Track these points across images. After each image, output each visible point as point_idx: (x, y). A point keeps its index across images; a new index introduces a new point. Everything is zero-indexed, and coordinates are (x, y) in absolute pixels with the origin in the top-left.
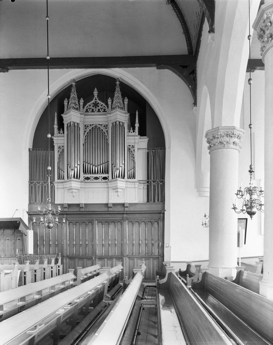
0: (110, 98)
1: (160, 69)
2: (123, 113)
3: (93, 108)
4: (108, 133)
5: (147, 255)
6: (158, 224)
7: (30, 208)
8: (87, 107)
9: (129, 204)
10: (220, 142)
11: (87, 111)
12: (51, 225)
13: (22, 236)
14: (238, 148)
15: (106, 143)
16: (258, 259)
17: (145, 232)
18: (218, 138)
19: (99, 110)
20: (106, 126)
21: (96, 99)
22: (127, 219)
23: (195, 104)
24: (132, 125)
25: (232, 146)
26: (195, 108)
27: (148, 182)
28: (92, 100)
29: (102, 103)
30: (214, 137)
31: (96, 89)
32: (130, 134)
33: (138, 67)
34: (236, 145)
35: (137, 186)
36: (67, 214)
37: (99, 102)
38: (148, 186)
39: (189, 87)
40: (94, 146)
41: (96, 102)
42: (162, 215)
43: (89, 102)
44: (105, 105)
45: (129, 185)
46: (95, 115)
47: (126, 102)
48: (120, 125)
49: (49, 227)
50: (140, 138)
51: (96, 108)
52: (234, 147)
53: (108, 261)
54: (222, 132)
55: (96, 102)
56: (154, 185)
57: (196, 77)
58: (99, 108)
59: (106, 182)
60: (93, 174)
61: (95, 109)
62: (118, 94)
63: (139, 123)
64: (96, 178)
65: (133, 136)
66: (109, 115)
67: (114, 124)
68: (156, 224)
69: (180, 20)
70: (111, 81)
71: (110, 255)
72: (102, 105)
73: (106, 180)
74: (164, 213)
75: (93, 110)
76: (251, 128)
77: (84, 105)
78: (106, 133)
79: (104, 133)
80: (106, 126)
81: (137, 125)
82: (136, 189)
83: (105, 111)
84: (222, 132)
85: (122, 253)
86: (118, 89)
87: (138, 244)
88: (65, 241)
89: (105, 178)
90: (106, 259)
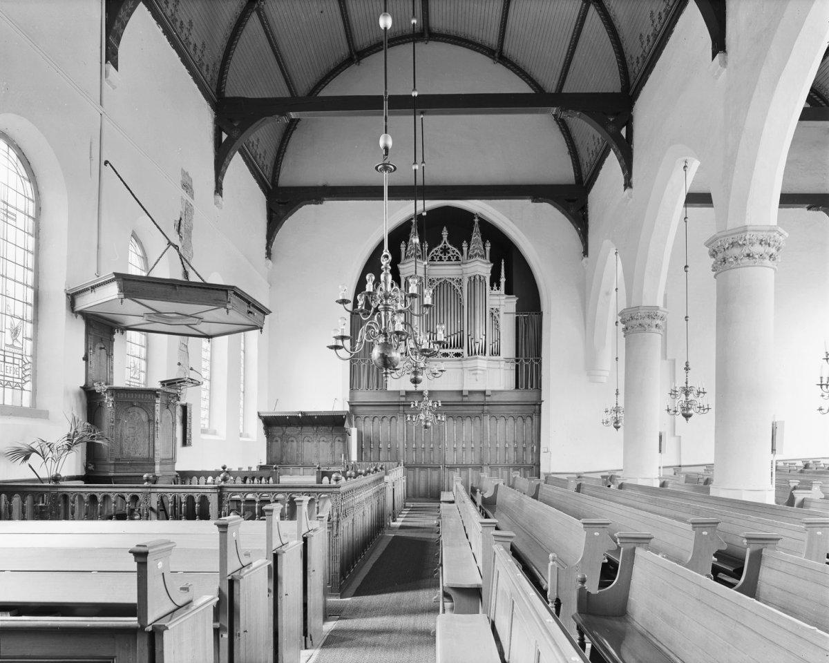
0: (465, 242)
1: (536, 202)
2: (483, 263)
3: (440, 255)
4: (462, 291)
6: (532, 420)
7: (352, 397)
8: (433, 253)
9: (492, 391)
10: (640, 325)
11: (432, 259)
12: (429, 424)
13: (345, 435)
15: (459, 305)
16: (672, 469)
17: (513, 431)
19: (449, 258)
20: (460, 281)
21: (445, 243)
23: (586, 253)
24: (495, 280)
25: (654, 329)
26: (585, 259)
27: (517, 361)
28: (440, 244)
29: (454, 249)
30: (632, 318)
31: (445, 229)
32: (493, 292)
33: (506, 199)
34: (659, 328)
35: (502, 366)
36: (404, 405)
37: (450, 246)
38: (517, 366)
39: (577, 230)
40: (442, 309)
41: (445, 246)
42: (537, 407)
43: (436, 247)
44: (458, 251)
45: (495, 365)
46: (445, 265)
47: (488, 249)
48: (480, 279)
49: (426, 427)
50: (507, 298)
51: (445, 255)
52: (657, 330)
53: (462, 472)
55: (445, 246)
56: (526, 365)
57: (587, 215)
58: (450, 255)
59: (460, 360)
60: (447, 347)
61: (443, 257)
62: (476, 237)
63: (506, 277)
64: (446, 355)
65: (498, 295)
66: (463, 266)
67: (472, 279)
68: (529, 419)
69: (564, 136)
70: (468, 216)
71: (464, 463)
72: (453, 251)
73: (459, 358)
74: (540, 405)
75: (441, 258)
77: (429, 250)
78: (459, 291)
79: (456, 291)
80: (460, 281)
81: (503, 280)
82: (502, 370)
83: (458, 259)
84: (642, 313)
85: (481, 460)
86: (476, 229)
89: (457, 355)
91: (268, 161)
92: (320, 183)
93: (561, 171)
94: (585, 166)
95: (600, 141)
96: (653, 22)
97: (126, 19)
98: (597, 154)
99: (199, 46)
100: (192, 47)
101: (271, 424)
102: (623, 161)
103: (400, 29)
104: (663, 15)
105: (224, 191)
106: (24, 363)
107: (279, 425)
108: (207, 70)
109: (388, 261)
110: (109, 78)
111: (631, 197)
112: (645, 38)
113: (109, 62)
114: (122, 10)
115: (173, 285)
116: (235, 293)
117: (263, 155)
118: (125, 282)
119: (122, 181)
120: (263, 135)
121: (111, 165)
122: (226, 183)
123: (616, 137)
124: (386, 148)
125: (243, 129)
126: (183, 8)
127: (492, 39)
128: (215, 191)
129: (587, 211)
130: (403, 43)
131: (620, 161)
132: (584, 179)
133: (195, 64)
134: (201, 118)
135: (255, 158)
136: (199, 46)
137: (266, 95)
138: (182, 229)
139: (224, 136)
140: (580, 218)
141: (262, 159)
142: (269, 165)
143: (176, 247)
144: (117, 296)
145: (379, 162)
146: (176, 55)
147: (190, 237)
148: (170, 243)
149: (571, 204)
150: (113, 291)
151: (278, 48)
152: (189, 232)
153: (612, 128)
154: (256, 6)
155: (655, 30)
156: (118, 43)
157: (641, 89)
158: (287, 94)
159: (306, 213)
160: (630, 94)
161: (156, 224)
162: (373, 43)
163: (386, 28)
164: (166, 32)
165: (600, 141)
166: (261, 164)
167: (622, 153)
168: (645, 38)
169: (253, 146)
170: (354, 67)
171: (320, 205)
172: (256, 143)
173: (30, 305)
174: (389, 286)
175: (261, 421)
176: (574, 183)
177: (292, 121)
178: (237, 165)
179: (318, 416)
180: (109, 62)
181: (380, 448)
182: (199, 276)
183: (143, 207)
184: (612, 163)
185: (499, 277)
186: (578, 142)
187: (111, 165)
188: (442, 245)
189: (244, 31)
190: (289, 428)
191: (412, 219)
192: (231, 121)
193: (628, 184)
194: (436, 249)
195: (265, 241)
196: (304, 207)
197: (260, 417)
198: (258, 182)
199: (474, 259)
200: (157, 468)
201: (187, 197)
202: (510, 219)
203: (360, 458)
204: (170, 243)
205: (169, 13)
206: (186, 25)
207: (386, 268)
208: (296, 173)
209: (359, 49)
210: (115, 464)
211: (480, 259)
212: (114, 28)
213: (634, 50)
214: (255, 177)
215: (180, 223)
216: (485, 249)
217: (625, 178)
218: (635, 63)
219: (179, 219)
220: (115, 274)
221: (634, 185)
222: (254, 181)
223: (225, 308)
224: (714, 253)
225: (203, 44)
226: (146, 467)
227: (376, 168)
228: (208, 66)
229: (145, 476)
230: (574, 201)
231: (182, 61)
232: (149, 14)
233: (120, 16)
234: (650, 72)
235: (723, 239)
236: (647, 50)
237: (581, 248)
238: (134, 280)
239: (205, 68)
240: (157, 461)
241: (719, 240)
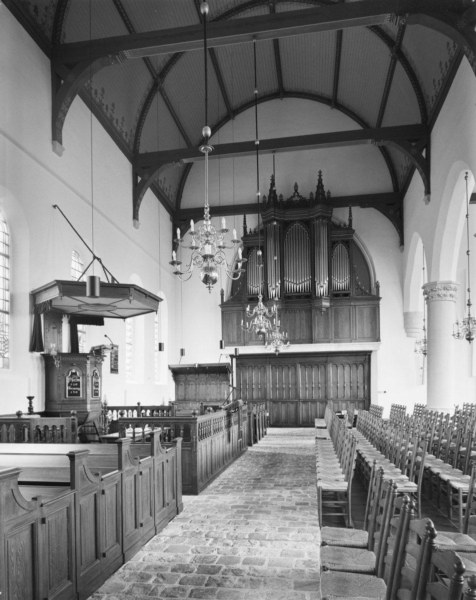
5: (352, 397)
10: (438, 295)
14: (454, 299)
18: (436, 291)
22: (332, 362)
23: (402, 243)
25: (448, 298)
30: (432, 290)
34: (453, 297)
42: (367, 356)
52: (451, 299)
54: (439, 286)
71: (313, 398)
76: (468, 255)
85: (326, 397)
87: (343, 387)
88: (268, 385)
90: (309, 403)
97: (66, 109)
101: (178, 373)
102: (423, 174)
104: (448, 64)
106: (4, 341)
107: (183, 374)
112: (437, 82)
116: (135, 289)
117: (163, 180)
120: (167, 175)
123: (418, 157)
127: (328, 91)
134: (122, 167)
139: (139, 179)
141: (163, 184)
143: (99, 259)
144: (58, 295)
148: (95, 257)
150: (55, 293)
154: (159, 87)
155: (443, 75)
161: (86, 245)
167: (422, 168)
168: (437, 82)
170: (230, 122)
173: (8, 301)
175: (170, 371)
178: (149, 198)
179: (209, 367)
181: (253, 389)
184: (417, 179)
190: (190, 376)
197: (170, 368)
200: (89, 406)
203: (24, 430)
204: (95, 257)
208: (188, 201)
210: (61, 404)
218: (431, 101)
220: (56, 281)
223: (128, 299)
226: (81, 405)
228: (126, 133)
229: (72, 412)
233: (62, 108)
240: (88, 402)
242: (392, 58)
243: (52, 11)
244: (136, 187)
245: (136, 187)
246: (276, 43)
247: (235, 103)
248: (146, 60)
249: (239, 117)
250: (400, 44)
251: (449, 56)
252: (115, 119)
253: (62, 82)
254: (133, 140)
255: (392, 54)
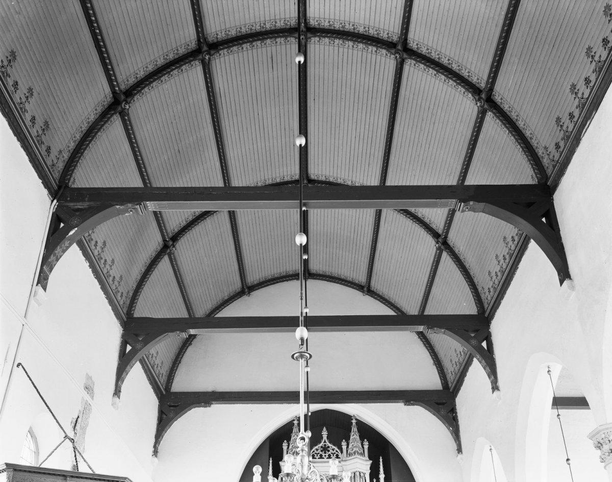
0: (344, 441)
3: (321, 453)
8: (314, 451)
21: (325, 442)
23: (459, 450)
26: (460, 456)
28: (320, 442)
29: (334, 447)
31: (325, 429)
37: (330, 445)
39: (449, 429)
47: (366, 447)
48: (360, 476)
55: (325, 445)
58: (330, 453)
61: (324, 455)
62: (355, 436)
66: (343, 463)
72: (333, 450)
75: (321, 456)
86: (354, 429)
91: (164, 370)
92: (210, 389)
93: (430, 380)
94: (450, 374)
95: (462, 353)
96: (499, 262)
98: (461, 364)
99: (117, 278)
100: (111, 278)
103: (284, 270)
105: (122, 394)
108: (122, 296)
109: (304, 443)
110: (37, 297)
111: (500, 399)
112: (493, 274)
113: (39, 285)
114: (59, 247)
115: (64, 476)
117: (160, 365)
118: (15, 472)
119: (31, 380)
121: (23, 367)
122: (124, 387)
123: (480, 349)
124: (302, 339)
125: (146, 342)
126: (108, 250)
127: (362, 278)
128: (114, 394)
129: (456, 413)
130: (287, 281)
131: (485, 369)
132: (450, 385)
133: (112, 291)
134: (114, 331)
135: (153, 367)
136: (117, 278)
137: (168, 316)
138: (78, 427)
139: (129, 348)
140: (450, 418)
141: (159, 368)
142: (165, 373)
143: (72, 440)
145: (296, 349)
146: (98, 283)
147: (84, 433)
148: (66, 437)
149: (440, 406)
151: (182, 282)
152: (84, 429)
153: (474, 342)
154: (120, 109)
156: (51, 271)
157: (495, 311)
158: (186, 316)
159: (195, 414)
160: (486, 315)
162: (261, 280)
163: (301, 245)
164: (92, 266)
165: (462, 353)
166: (152, 363)
169: (152, 357)
170: (245, 298)
171: (208, 408)
172: (155, 355)
174: (306, 468)
176: (442, 389)
177: (191, 336)
178: (136, 373)
180: (39, 285)
182: (91, 469)
183: (46, 404)
184: (477, 369)
185: (378, 473)
186: (441, 354)
187: (23, 367)
188: (322, 444)
189: (156, 269)
191: (294, 420)
192: (137, 335)
193: (495, 388)
194: (317, 447)
195: (154, 440)
196: (193, 410)
198: (153, 388)
199: (353, 457)
201: (87, 397)
202: (386, 420)
204: (66, 437)
205: (96, 253)
206: (109, 262)
207: (302, 450)
209: (250, 284)
211: (359, 457)
212: (49, 260)
213: (486, 284)
214: (151, 383)
215: (76, 421)
216: (363, 447)
217: (492, 382)
218: (487, 293)
219: (77, 417)
220: (7, 464)
221: (501, 388)
222: (150, 387)
224: (599, 445)
225: (121, 276)
227: (293, 356)
230: (443, 404)
231: (101, 288)
232: (80, 253)
233: (56, 252)
234: (502, 298)
235: (606, 431)
236: (497, 282)
237: (454, 446)
238: (25, 471)
239: (119, 294)
241: (602, 433)
242: (437, 249)
243: (66, 156)
244: (53, 233)
245: (53, 233)
246: (379, 214)
247: (252, 278)
248: (157, 216)
249: (256, 294)
250: (446, 237)
251: (499, 267)
252: (94, 240)
253: (62, 225)
254: (166, 380)
255: (437, 245)
